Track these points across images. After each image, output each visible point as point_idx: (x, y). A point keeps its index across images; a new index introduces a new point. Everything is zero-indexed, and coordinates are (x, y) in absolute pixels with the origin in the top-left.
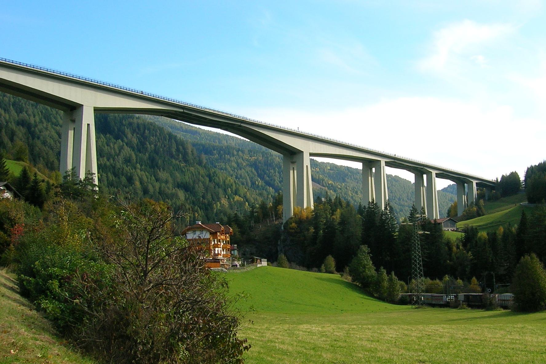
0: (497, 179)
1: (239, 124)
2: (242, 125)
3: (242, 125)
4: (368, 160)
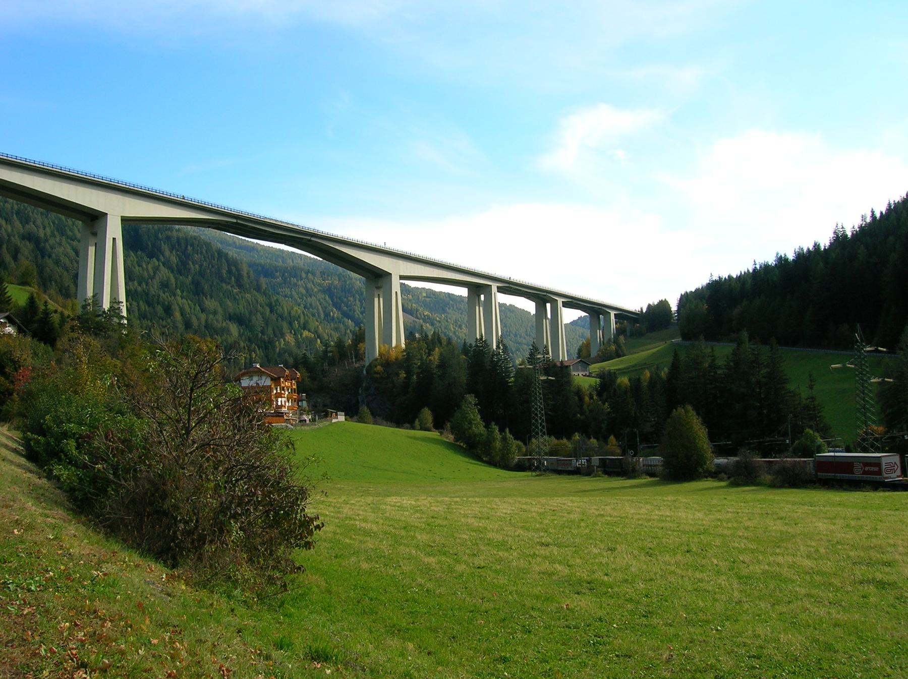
0: (642, 309)
2: (312, 239)
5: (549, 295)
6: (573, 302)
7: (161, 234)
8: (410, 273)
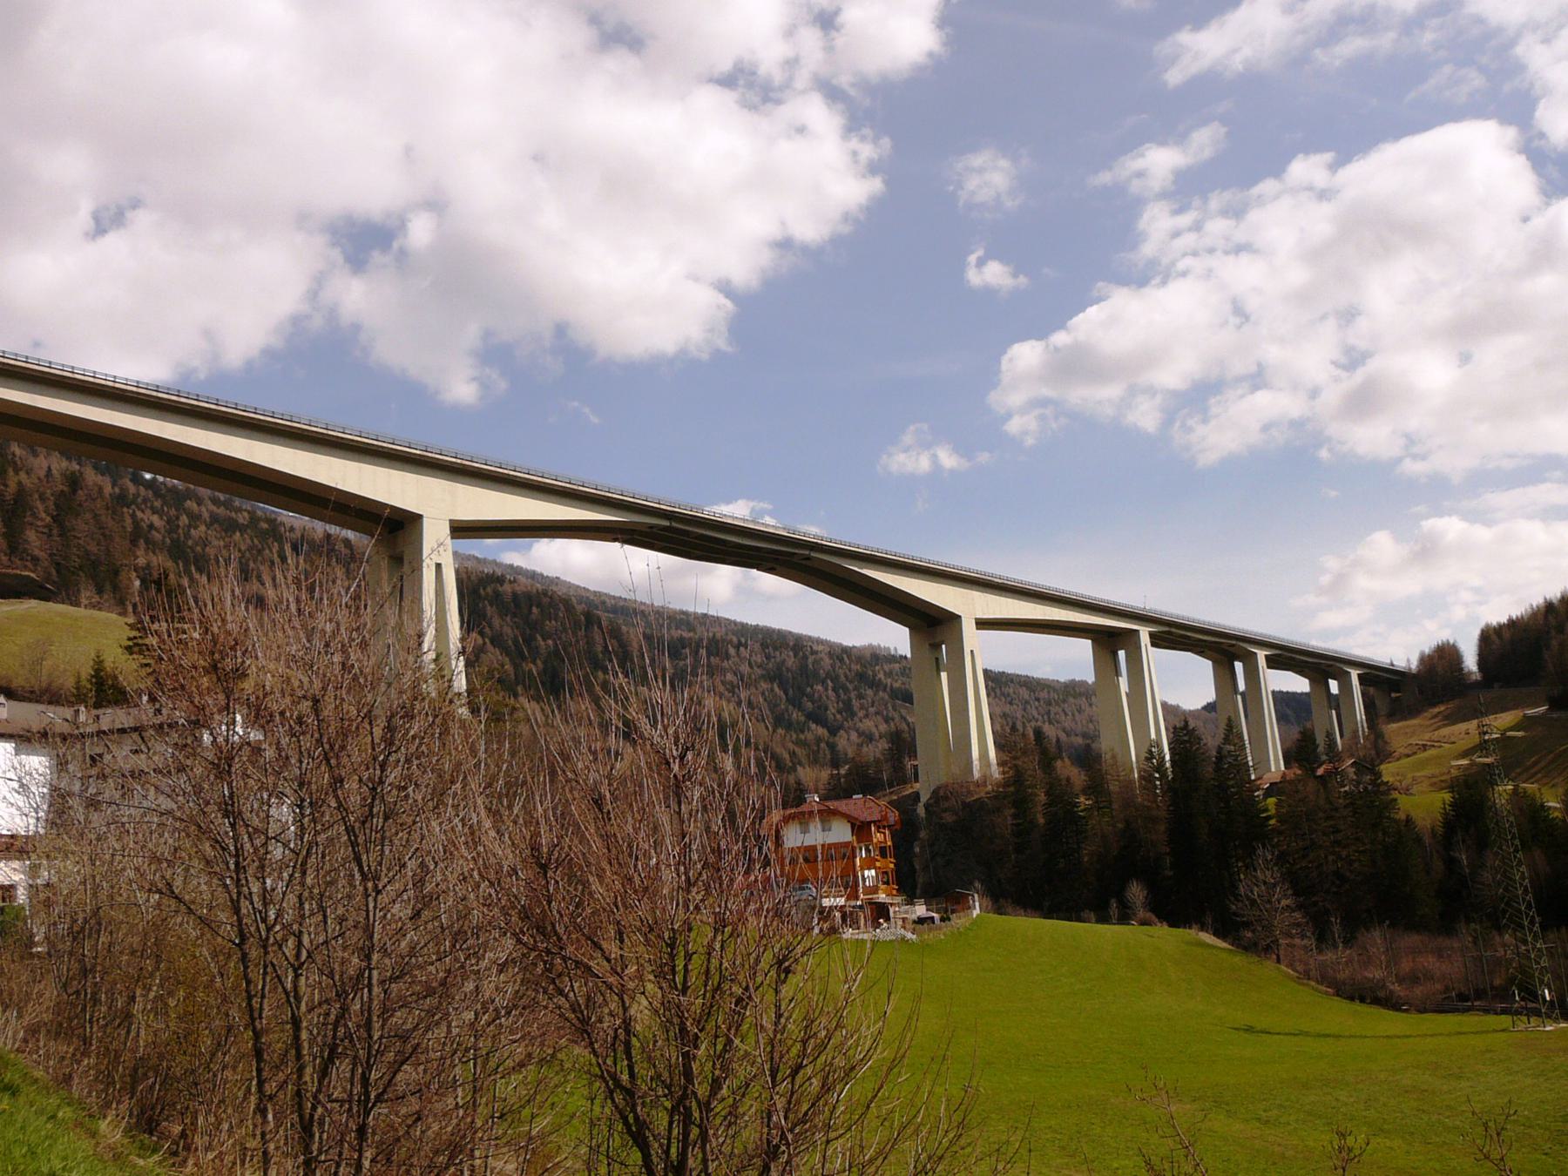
0: (1408, 660)
1: (807, 552)
2: (813, 554)
3: (813, 554)
4: (1101, 631)
5: (1241, 644)
6: (1287, 657)
7: (484, 589)
8: (994, 614)
